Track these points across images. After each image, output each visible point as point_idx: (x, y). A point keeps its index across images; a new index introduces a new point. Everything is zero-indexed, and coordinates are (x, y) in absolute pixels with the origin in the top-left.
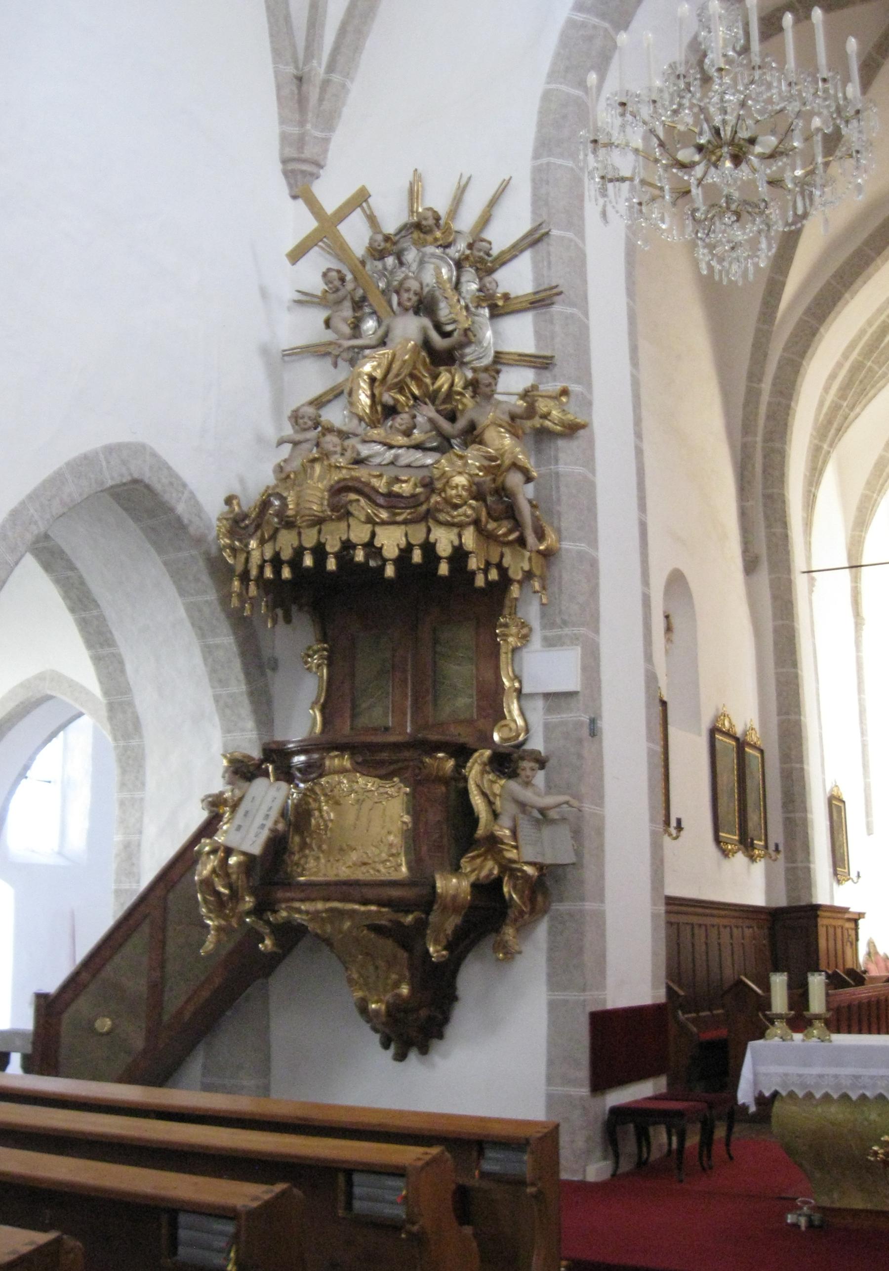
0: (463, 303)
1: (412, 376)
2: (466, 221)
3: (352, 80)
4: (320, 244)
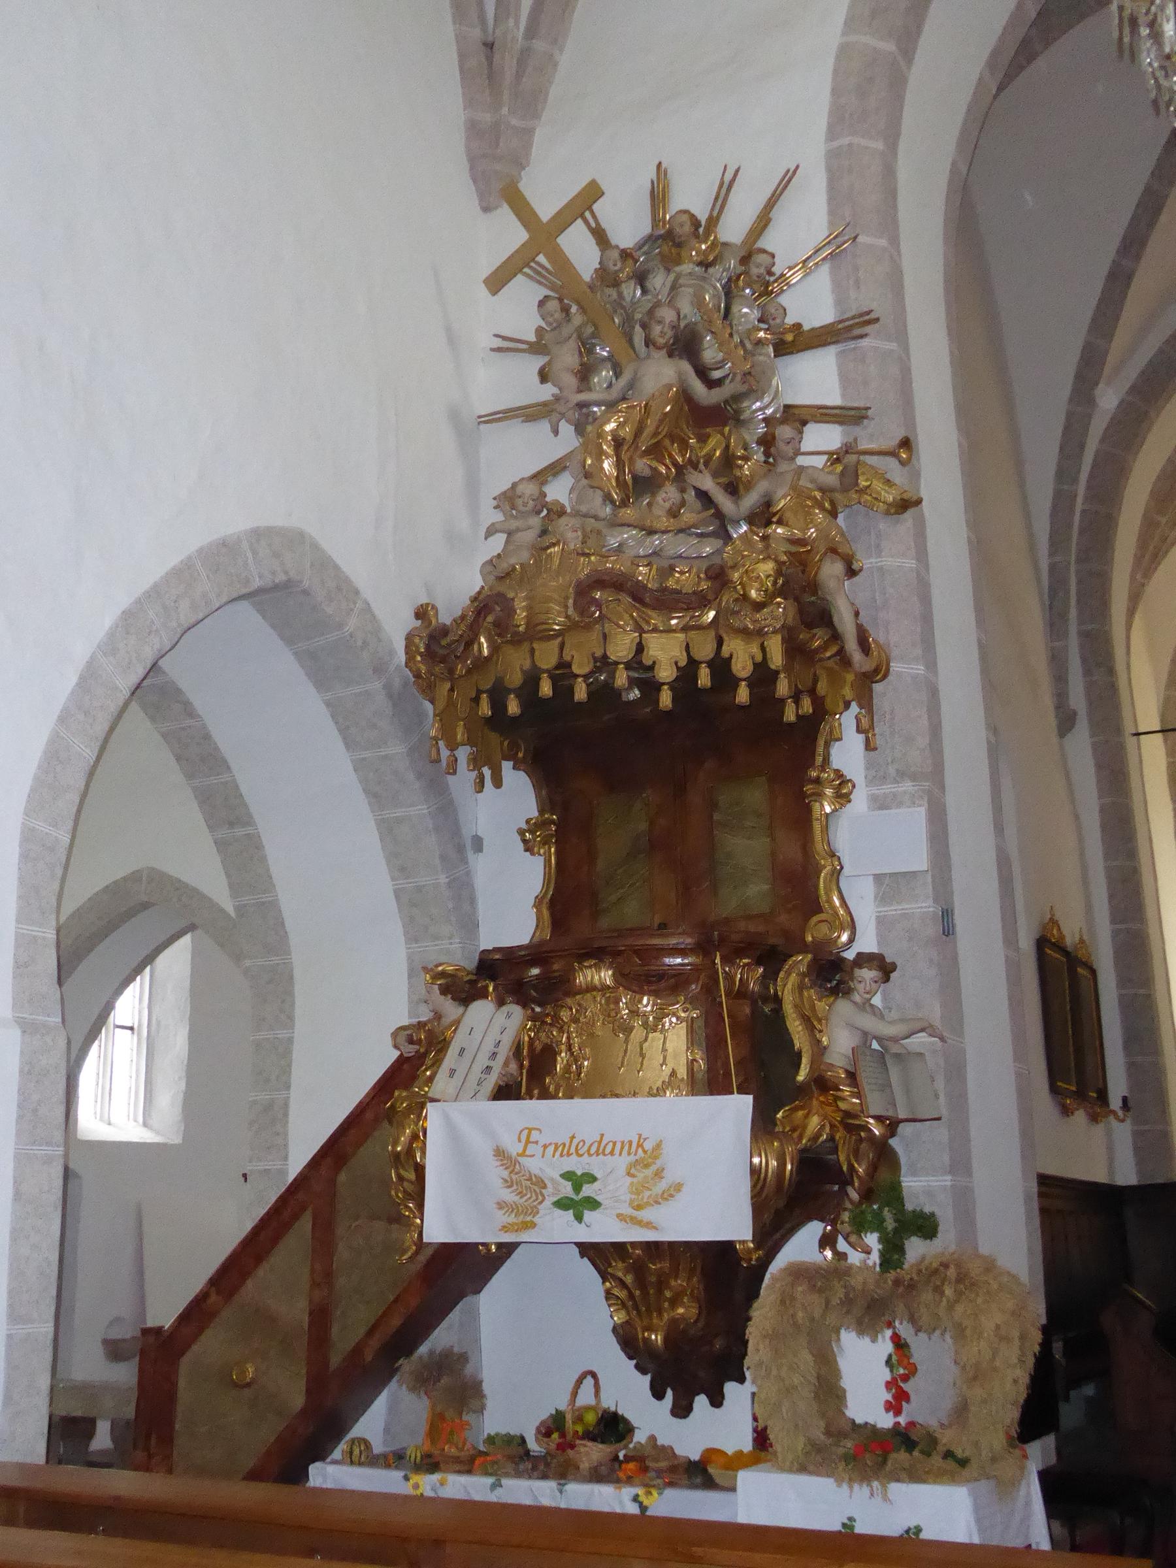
0: (737, 339)
1: (672, 438)
2: (733, 229)
3: (561, 50)
4: (526, 270)
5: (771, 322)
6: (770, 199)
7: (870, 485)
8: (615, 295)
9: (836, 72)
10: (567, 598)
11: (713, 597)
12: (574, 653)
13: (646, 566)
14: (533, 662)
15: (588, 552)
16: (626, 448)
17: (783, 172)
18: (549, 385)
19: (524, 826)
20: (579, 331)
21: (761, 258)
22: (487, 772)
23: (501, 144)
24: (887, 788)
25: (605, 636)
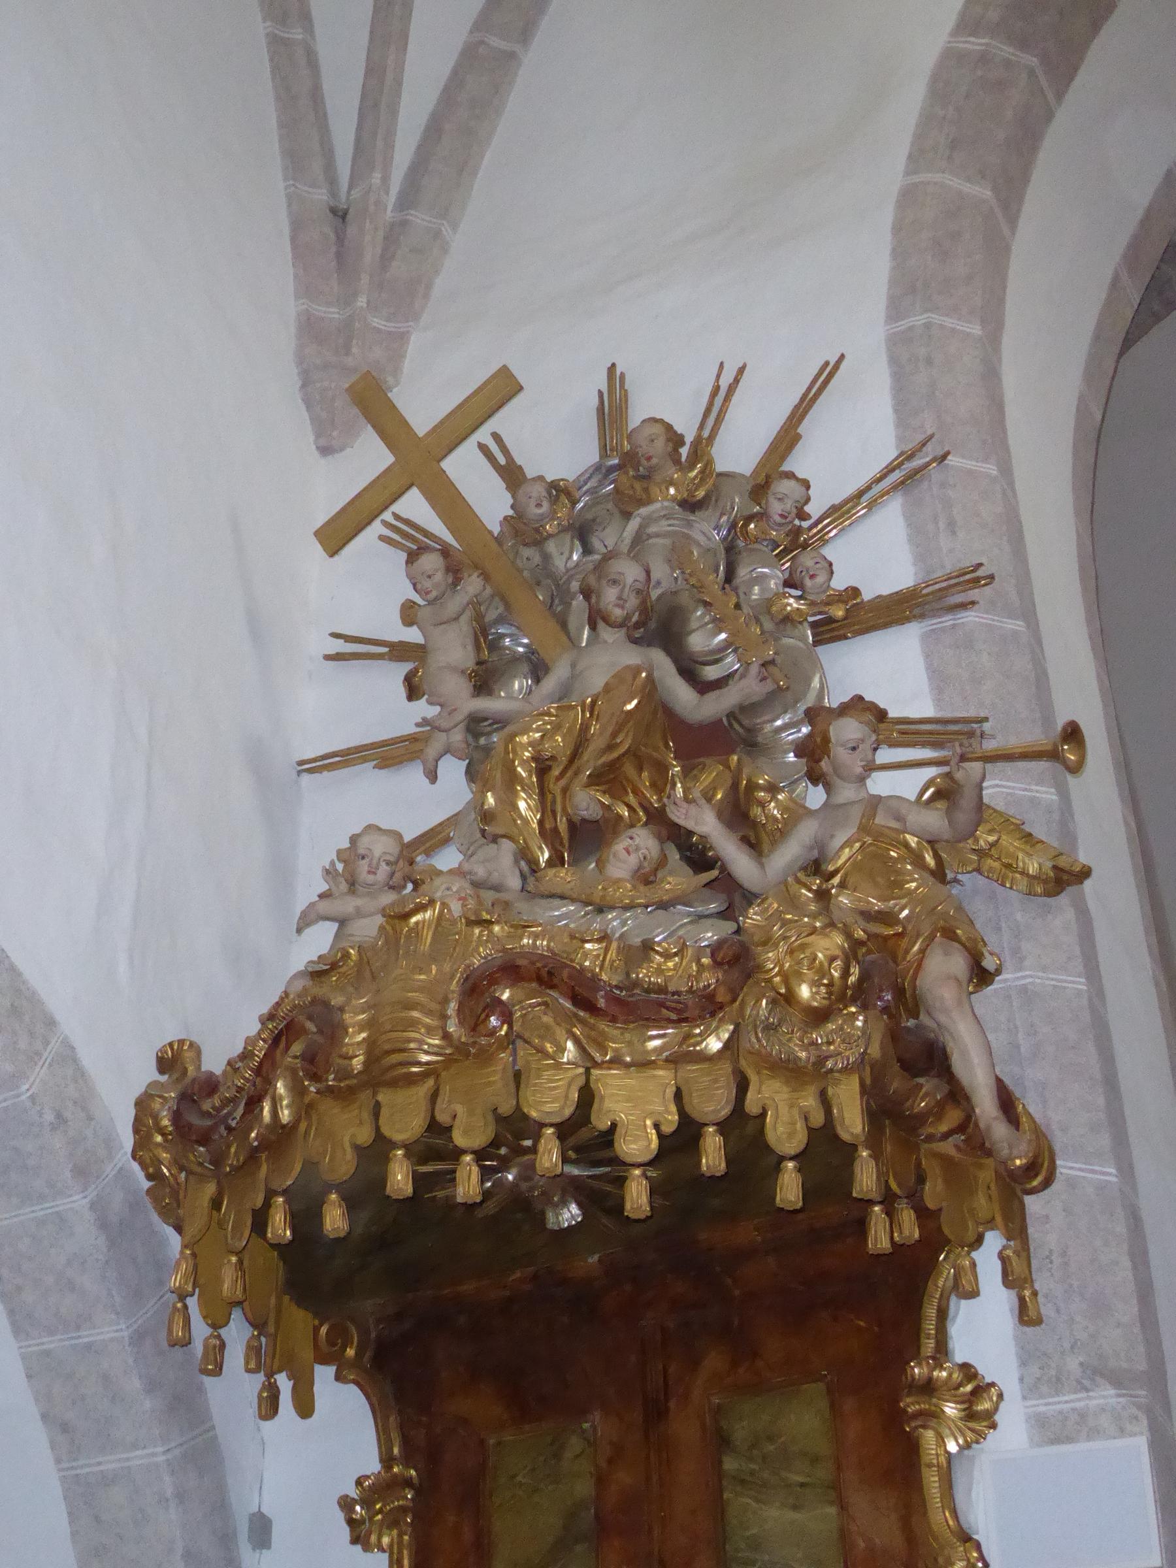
3: (455, 226)
5: (808, 583)
6: (797, 407)
7: (997, 841)
8: (537, 559)
9: (897, 229)
10: (445, 1001)
11: (728, 998)
12: (460, 1109)
13: (599, 941)
14: (378, 1128)
15: (488, 917)
16: (556, 772)
17: (821, 363)
18: (422, 702)
19: (353, 1493)
20: (475, 603)
21: (785, 487)
22: (284, 1383)
23: (354, 350)
24: (1068, 1401)
25: (517, 1076)
